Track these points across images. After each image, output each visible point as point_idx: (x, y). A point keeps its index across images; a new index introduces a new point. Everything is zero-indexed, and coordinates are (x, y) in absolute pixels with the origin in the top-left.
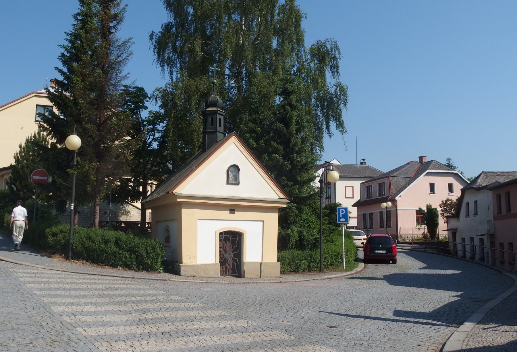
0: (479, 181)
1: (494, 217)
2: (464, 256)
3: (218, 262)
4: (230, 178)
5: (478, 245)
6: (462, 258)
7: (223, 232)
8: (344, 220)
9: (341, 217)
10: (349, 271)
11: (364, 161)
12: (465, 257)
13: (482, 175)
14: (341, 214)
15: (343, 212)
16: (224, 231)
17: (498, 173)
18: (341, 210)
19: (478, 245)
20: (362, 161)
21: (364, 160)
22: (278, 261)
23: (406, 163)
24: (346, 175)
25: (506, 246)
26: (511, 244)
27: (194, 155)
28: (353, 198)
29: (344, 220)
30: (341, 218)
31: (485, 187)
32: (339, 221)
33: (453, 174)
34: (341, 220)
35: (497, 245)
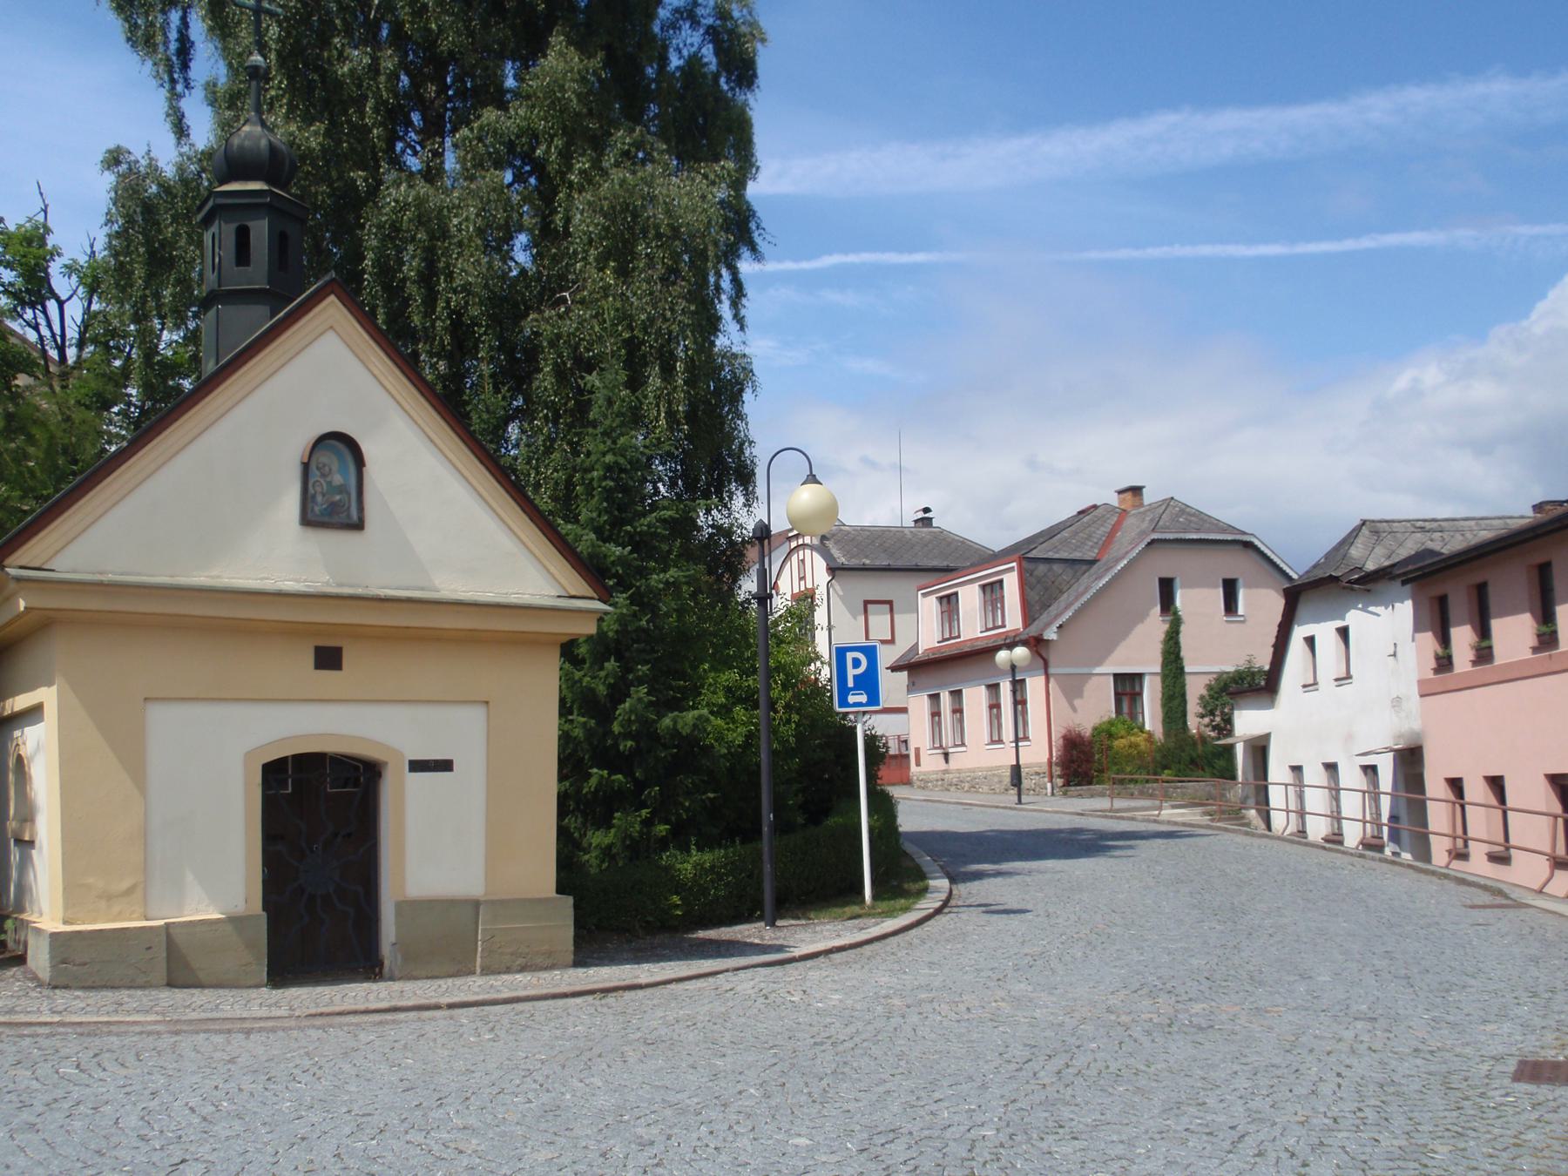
0: (1356, 552)
1: (1421, 683)
2: (1335, 839)
3: (257, 906)
4: (319, 499)
5: (1389, 791)
6: (1328, 845)
7: (286, 758)
8: (863, 698)
9: (851, 684)
10: (890, 914)
11: (927, 515)
12: (1341, 843)
13: (1365, 530)
14: (851, 672)
15: (856, 663)
16: (295, 757)
17: (1419, 524)
18: (850, 656)
19: (1389, 791)
20: (921, 515)
21: (927, 510)
22: (561, 889)
23: (1075, 513)
24: (868, 562)
25: (1476, 790)
26: (1496, 784)
27: (756, 773)
28: (892, 641)
29: (863, 698)
30: (851, 689)
31: (1382, 575)
32: (843, 703)
33: (1240, 547)
34: (852, 699)
35: (1435, 786)
